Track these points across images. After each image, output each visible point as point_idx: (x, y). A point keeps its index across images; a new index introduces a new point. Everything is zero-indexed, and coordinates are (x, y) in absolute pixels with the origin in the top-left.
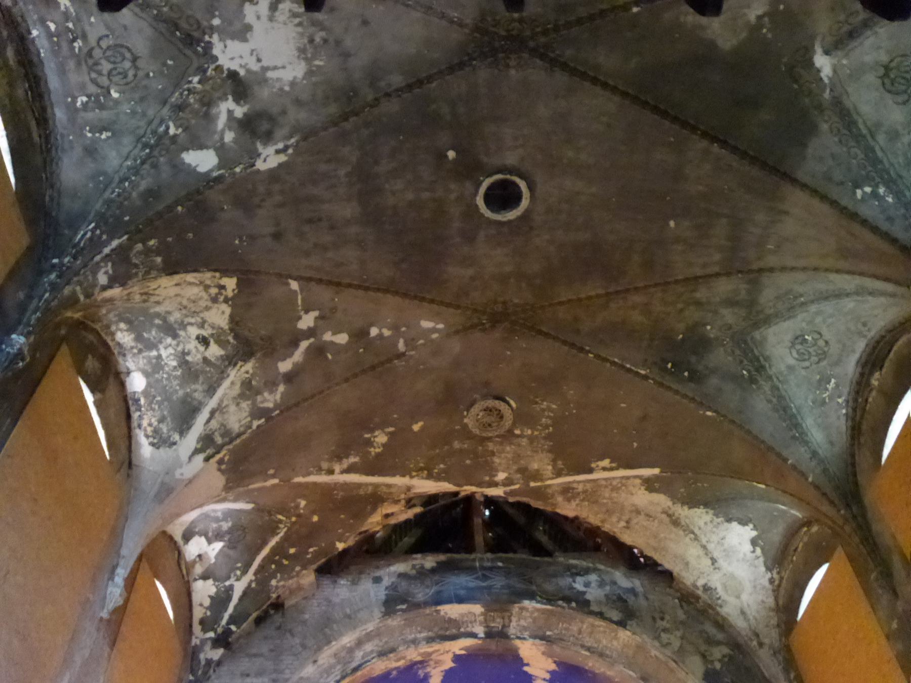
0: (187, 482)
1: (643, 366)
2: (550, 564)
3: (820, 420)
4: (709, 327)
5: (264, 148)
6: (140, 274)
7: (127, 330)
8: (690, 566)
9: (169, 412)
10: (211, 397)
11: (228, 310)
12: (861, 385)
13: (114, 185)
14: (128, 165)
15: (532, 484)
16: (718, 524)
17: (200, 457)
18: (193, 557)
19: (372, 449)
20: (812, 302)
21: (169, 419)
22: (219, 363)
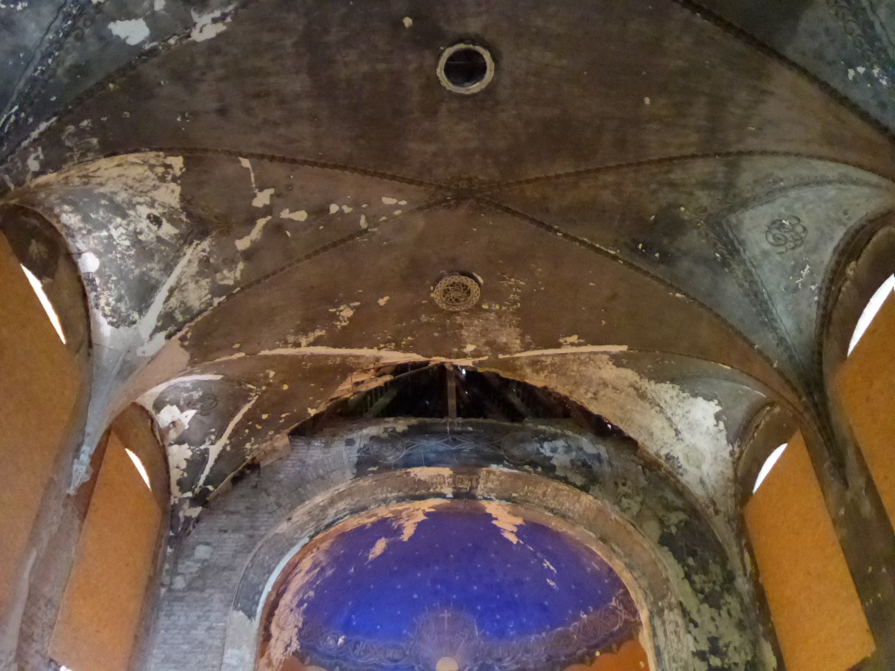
0: (150, 359)
1: (613, 246)
2: (518, 430)
3: (790, 307)
4: (682, 209)
5: (200, 17)
6: (75, 158)
7: (72, 212)
8: (654, 436)
9: (126, 291)
10: (169, 276)
11: (178, 189)
12: (836, 274)
13: (36, 62)
14: (49, 39)
15: (501, 356)
16: (684, 398)
17: (162, 335)
18: (166, 424)
19: (338, 323)
20: (793, 187)
21: (127, 298)
22: (173, 242)
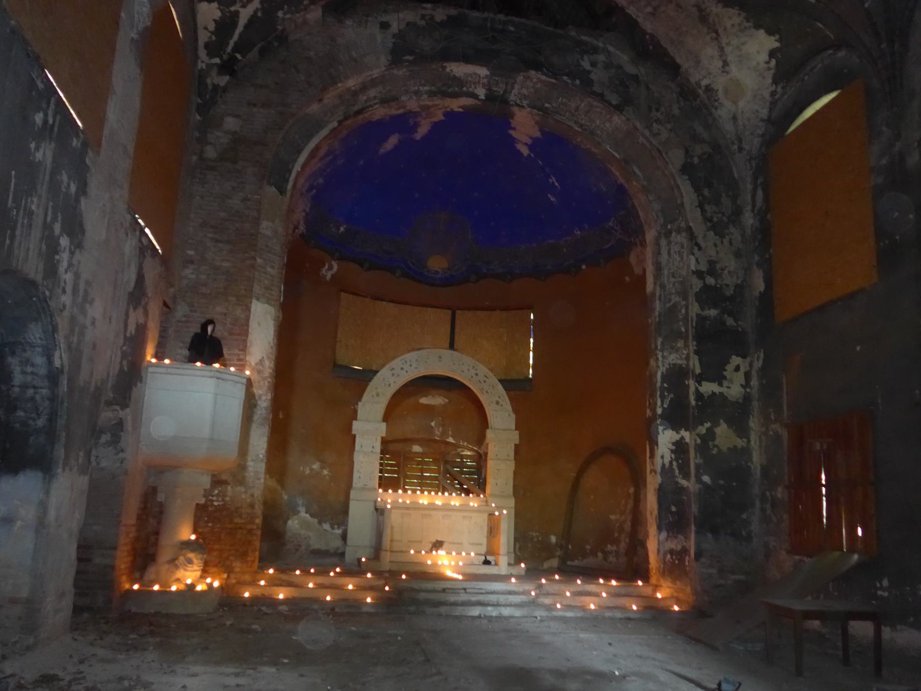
16: (746, 28)
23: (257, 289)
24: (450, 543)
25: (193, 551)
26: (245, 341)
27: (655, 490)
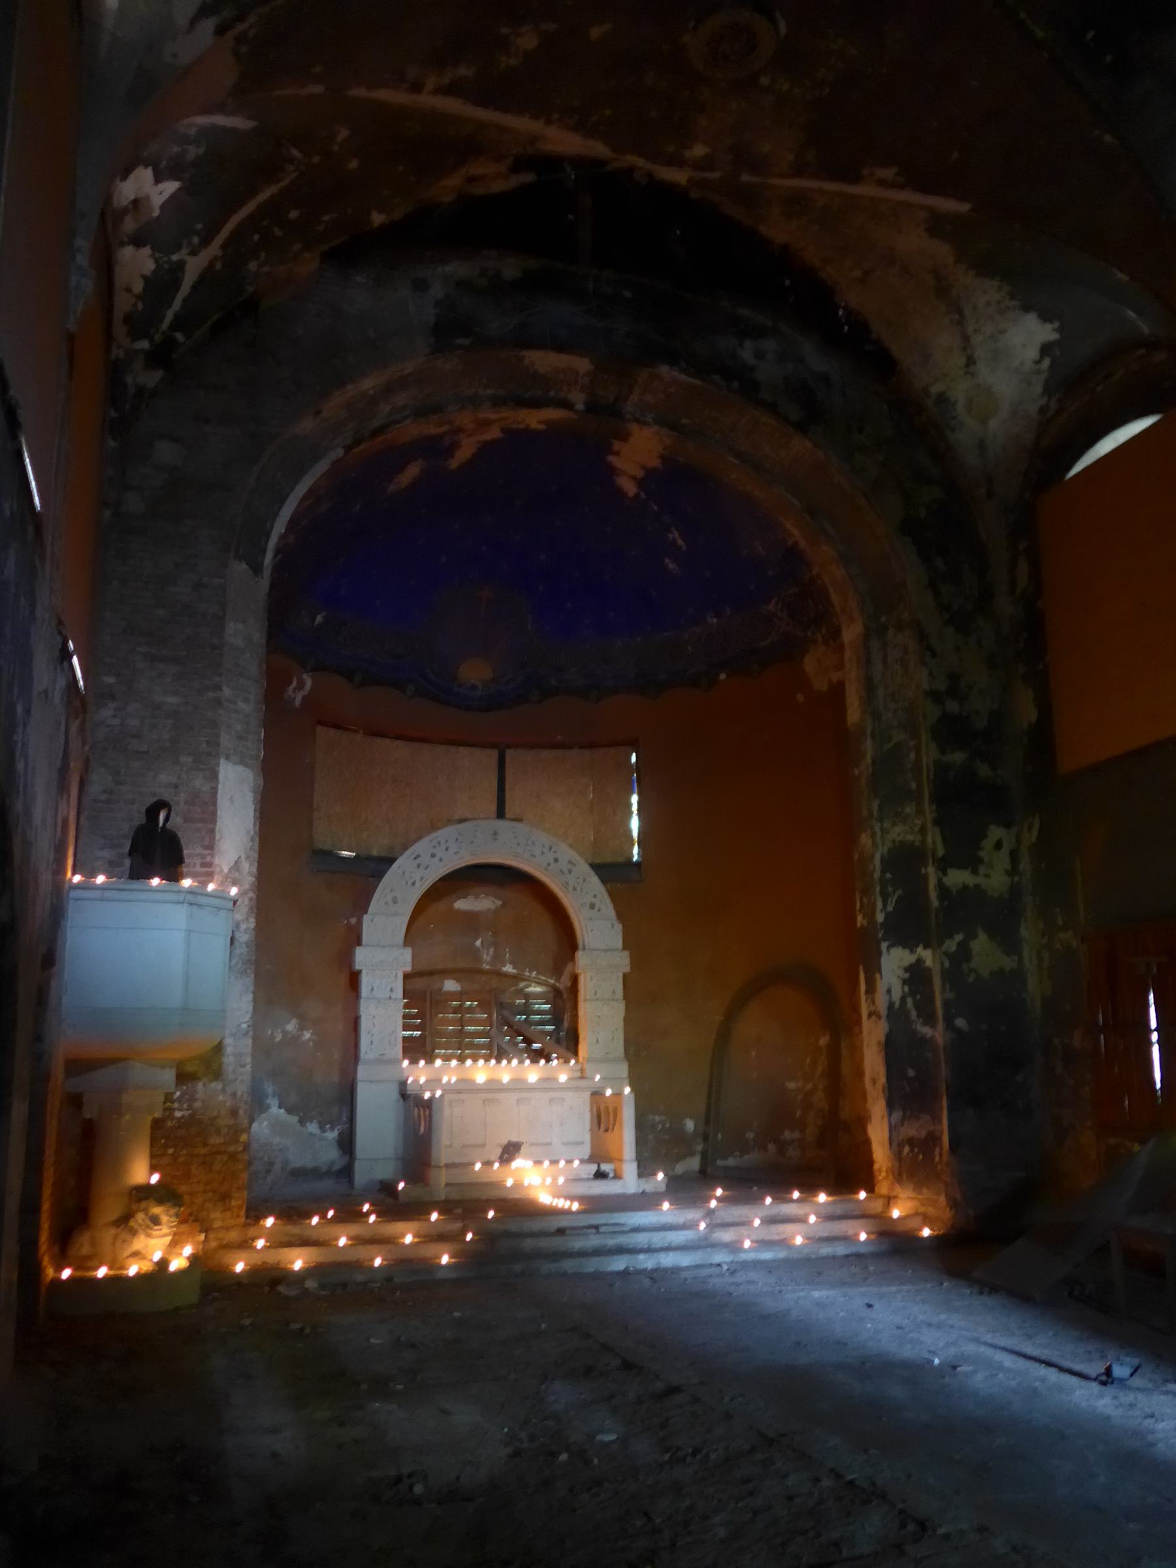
15: (745, 178)
17: (209, 25)
18: (124, 203)
23: (226, 740)
24: (532, 1144)
25: (160, 1201)
26: (212, 831)
27: (879, 1043)
